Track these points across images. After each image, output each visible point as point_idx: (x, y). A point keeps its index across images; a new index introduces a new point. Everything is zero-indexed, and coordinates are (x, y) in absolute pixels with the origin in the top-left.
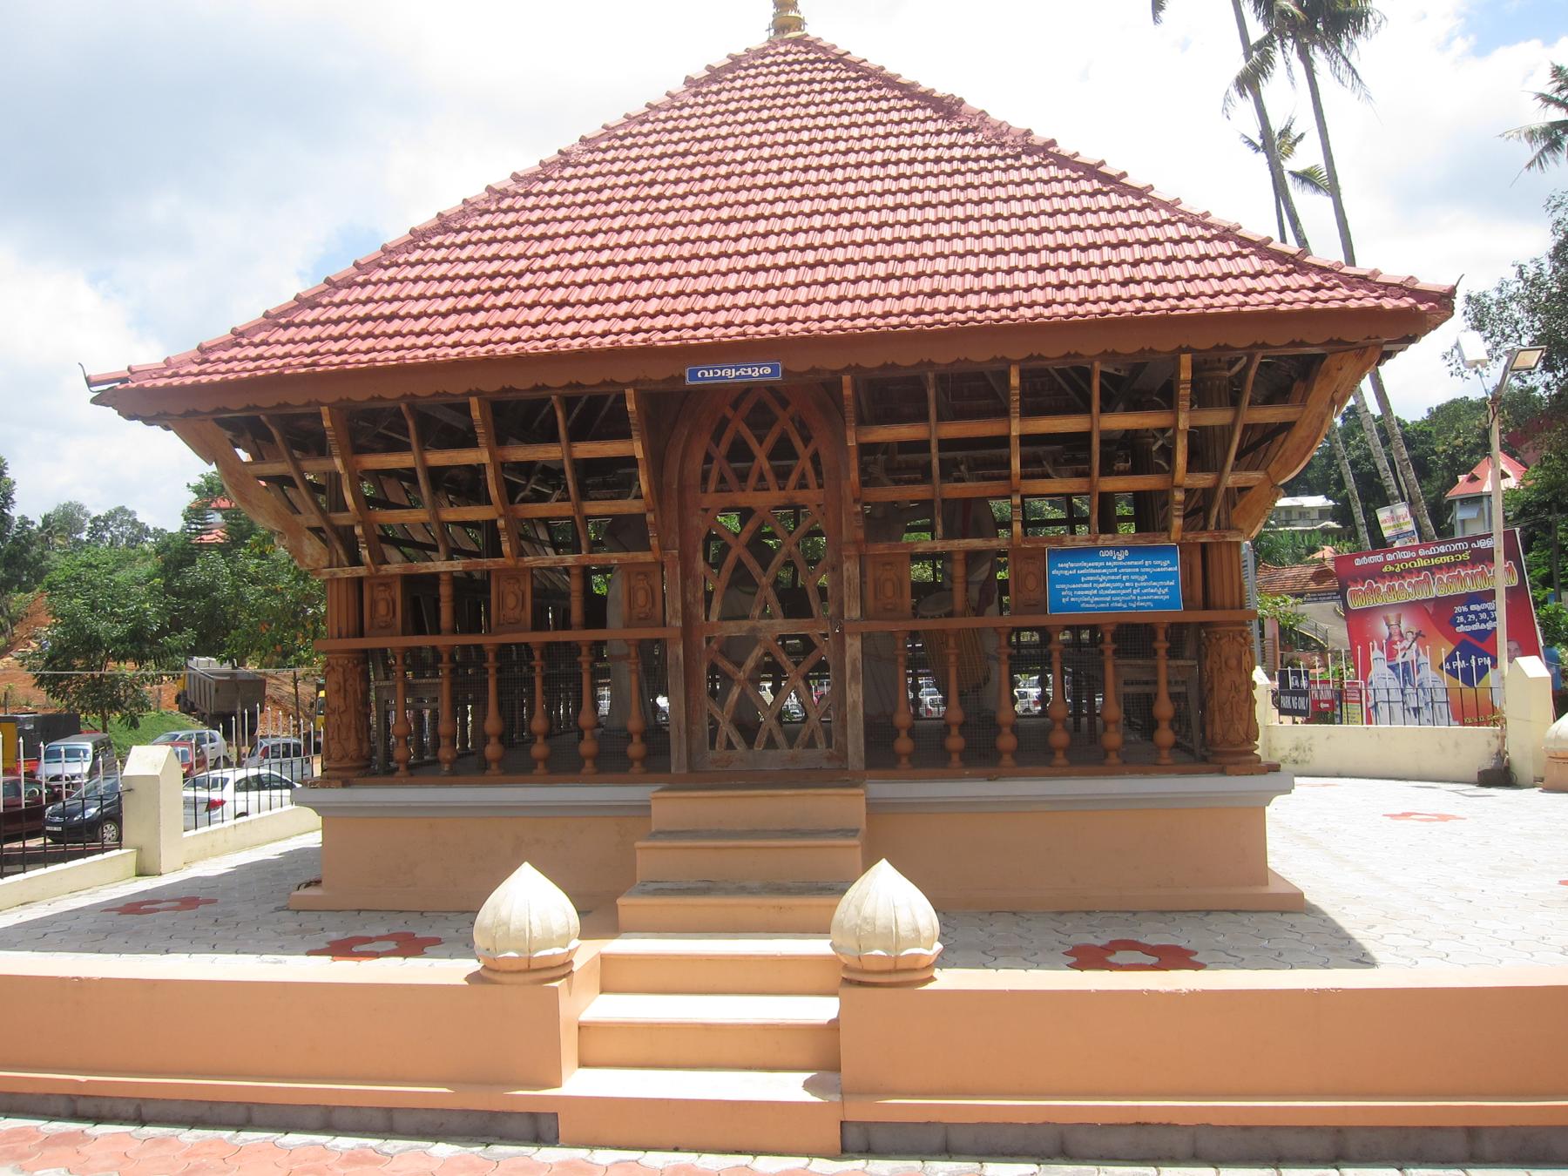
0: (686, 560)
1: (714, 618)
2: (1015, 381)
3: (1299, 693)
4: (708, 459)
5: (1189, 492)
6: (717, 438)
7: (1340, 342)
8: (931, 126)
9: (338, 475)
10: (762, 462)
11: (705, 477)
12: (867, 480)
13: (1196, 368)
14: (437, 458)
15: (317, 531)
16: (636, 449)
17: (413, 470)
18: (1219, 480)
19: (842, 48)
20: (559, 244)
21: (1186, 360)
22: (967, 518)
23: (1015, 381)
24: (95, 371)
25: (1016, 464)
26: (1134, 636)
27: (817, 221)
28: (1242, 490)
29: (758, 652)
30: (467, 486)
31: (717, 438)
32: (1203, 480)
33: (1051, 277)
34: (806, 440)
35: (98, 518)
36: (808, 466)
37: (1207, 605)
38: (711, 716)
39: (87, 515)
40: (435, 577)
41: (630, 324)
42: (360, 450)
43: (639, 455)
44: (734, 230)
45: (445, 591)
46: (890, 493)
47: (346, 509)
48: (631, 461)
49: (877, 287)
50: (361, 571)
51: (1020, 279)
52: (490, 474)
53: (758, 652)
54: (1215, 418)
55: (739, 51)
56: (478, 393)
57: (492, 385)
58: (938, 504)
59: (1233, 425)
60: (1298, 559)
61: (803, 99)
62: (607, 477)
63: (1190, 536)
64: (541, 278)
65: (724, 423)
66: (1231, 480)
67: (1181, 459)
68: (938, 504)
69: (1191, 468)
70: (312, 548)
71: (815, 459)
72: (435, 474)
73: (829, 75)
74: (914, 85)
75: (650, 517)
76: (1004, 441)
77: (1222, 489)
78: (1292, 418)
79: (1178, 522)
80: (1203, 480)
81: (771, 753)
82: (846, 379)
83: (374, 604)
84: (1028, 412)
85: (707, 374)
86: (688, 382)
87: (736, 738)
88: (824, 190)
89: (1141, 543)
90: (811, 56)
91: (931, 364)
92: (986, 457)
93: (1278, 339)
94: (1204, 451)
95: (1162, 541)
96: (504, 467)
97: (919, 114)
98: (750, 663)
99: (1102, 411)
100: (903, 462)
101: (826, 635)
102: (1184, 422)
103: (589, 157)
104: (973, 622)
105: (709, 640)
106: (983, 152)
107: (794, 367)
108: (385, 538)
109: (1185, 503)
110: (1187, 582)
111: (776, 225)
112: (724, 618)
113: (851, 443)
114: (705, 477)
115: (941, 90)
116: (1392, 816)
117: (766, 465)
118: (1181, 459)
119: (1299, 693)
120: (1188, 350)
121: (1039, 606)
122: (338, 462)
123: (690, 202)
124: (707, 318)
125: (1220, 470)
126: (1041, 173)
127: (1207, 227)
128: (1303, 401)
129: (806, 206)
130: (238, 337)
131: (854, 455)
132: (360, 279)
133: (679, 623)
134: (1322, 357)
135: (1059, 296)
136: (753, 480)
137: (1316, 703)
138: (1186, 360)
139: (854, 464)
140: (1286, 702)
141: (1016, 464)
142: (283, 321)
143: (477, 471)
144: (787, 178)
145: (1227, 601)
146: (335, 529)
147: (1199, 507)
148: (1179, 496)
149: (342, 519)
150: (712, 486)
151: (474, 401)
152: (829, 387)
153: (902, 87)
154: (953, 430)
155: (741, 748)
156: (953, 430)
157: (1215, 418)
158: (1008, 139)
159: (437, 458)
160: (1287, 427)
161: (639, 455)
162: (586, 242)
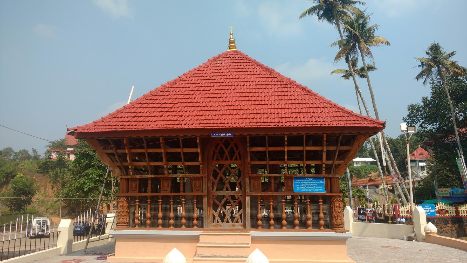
0: (208, 176)
1: (215, 191)
2: (286, 139)
3: (364, 214)
4: (214, 153)
5: (327, 165)
6: (216, 147)
7: (360, 133)
8: (267, 76)
9: (126, 154)
10: (227, 154)
11: (213, 157)
12: (252, 159)
13: (327, 136)
14: (150, 151)
15: (119, 167)
16: (199, 150)
17: (144, 153)
18: (333, 162)
19: (246, 54)
20: (180, 101)
21: (325, 135)
22: (275, 169)
23: (286, 139)
24: (69, 127)
25: (286, 157)
26: (314, 198)
27: (240, 99)
28: (339, 165)
29: (225, 199)
30: (157, 157)
31: (216, 147)
32: (330, 162)
33: (294, 115)
34: (237, 148)
35: (17, 153)
36: (238, 155)
37: (331, 192)
38: (213, 214)
39: (13, 152)
40: (148, 179)
41: (198, 122)
42: (131, 148)
43: (199, 152)
44: (221, 100)
45: (150, 182)
46: (257, 163)
47: (127, 162)
48: (197, 153)
49: (255, 116)
50: (129, 177)
51: (287, 115)
52: (163, 155)
53: (225, 199)
54: (332, 148)
55: (221, 53)
56: (162, 136)
57: (166, 135)
58: (268, 166)
59: (336, 151)
60: (365, 177)
61: (236, 67)
62: (194, 157)
63: (327, 175)
64: (176, 109)
65: (218, 144)
66: (336, 162)
67: (324, 157)
68: (268, 166)
69: (327, 159)
70: (117, 171)
71: (239, 153)
72: (149, 154)
73: (242, 61)
74: (263, 65)
75: (201, 166)
76: (283, 152)
77: (334, 165)
78: (350, 149)
79: (324, 172)
80: (330, 162)
81: (228, 224)
82: (248, 137)
83: (131, 185)
84: (288, 146)
85: (217, 135)
86: (212, 136)
87: (219, 220)
88: (242, 91)
89: (316, 176)
90: (238, 56)
91: (267, 134)
92: (279, 156)
93: (346, 132)
94: (330, 155)
95: (320, 176)
96: (167, 153)
97: (264, 73)
98: (223, 202)
99: (306, 146)
100: (261, 156)
101: (241, 196)
102: (325, 150)
103: (186, 79)
104: (275, 194)
105: (213, 196)
106: (279, 83)
107: (236, 134)
108: (137, 170)
109: (326, 167)
110: (326, 186)
111: (231, 99)
112: (217, 190)
113: (248, 151)
114: (213, 157)
115: (269, 66)
116: (383, 247)
117: (228, 155)
118: (324, 157)
119: (364, 214)
120: (325, 133)
121: (292, 190)
122: (127, 151)
123: (211, 92)
124: (216, 122)
125: (334, 160)
126: (293, 89)
127: (331, 104)
128: (352, 145)
129: (238, 95)
130: (103, 120)
131: (249, 154)
132: (132, 107)
133: (206, 192)
134: (357, 135)
135: (296, 120)
136: (224, 158)
137: (368, 217)
138: (325, 135)
139: (249, 155)
140: (360, 217)
141: (286, 157)
142: (114, 116)
143: (160, 154)
144: (233, 87)
145: (336, 191)
146: (123, 166)
147: (329, 168)
148: (324, 165)
149: (125, 164)
150: (215, 159)
151: (161, 138)
152: (244, 138)
153: (260, 65)
154: (272, 149)
155: (220, 222)
156: (272, 149)
157: (332, 148)
158: (285, 80)
159: (150, 151)
160: (349, 151)
161: (199, 152)
162: (187, 101)
